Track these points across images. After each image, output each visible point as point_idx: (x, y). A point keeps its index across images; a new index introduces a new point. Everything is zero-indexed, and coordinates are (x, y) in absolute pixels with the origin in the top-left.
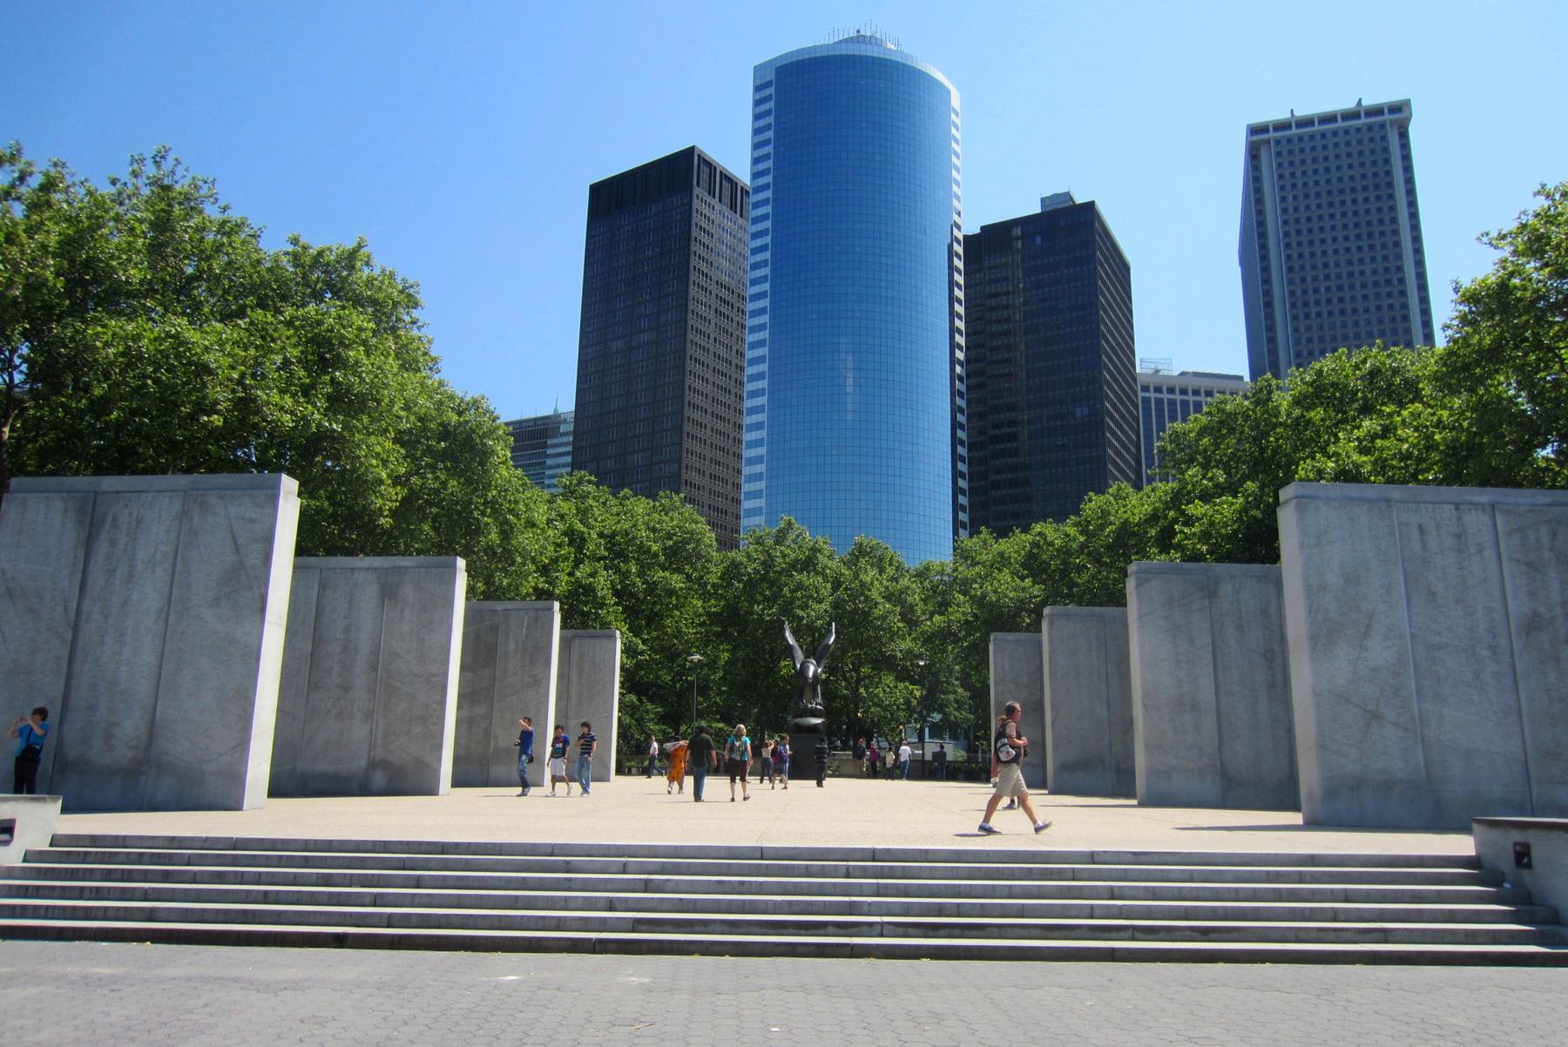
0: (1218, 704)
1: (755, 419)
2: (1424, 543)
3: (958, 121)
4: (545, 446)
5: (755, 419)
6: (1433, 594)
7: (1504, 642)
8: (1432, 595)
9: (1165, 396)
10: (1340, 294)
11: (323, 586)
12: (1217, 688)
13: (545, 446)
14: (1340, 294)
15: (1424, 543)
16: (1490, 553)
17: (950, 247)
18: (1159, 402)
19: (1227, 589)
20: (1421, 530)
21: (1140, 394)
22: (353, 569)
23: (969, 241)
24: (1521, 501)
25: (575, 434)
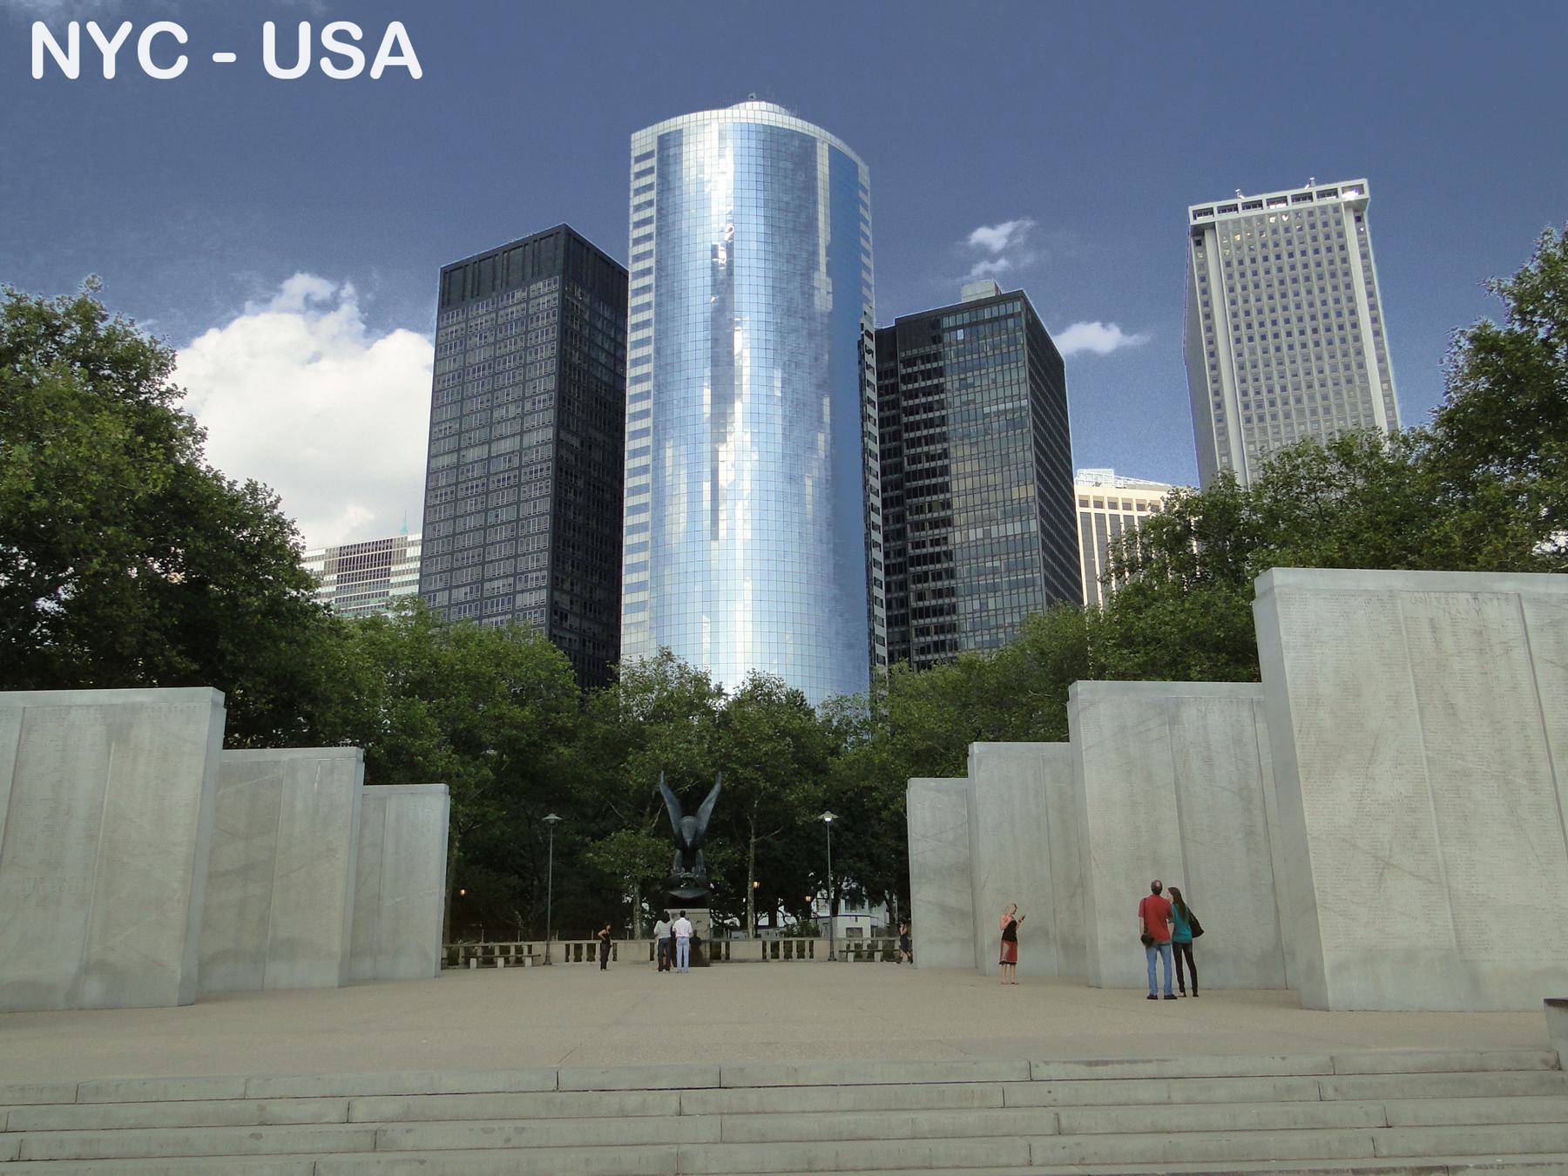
0: (1185, 856)
1: (641, 265)
2: (1437, 642)
3: (869, 247)
4: (388, 584)
5: (641, 265)
6: (1452, 706)
7: (1544, 768)
8: (1451, 709)
9: (1107, 511)
10: (1340, 320)
11: (26, 727)
12: (1182, 837)
13: (388, 584)
14: (1340, 320)
15: (1437, 642)
16: (1519, 653)
17: (861, 343)
18: (1101, 517)
19: (1189, 714)
20: (1434, 627)
21: (1079, 510)
22: (69, 707)
23: (882, 337)
24: (1554, 589)
25: (422, 559)
